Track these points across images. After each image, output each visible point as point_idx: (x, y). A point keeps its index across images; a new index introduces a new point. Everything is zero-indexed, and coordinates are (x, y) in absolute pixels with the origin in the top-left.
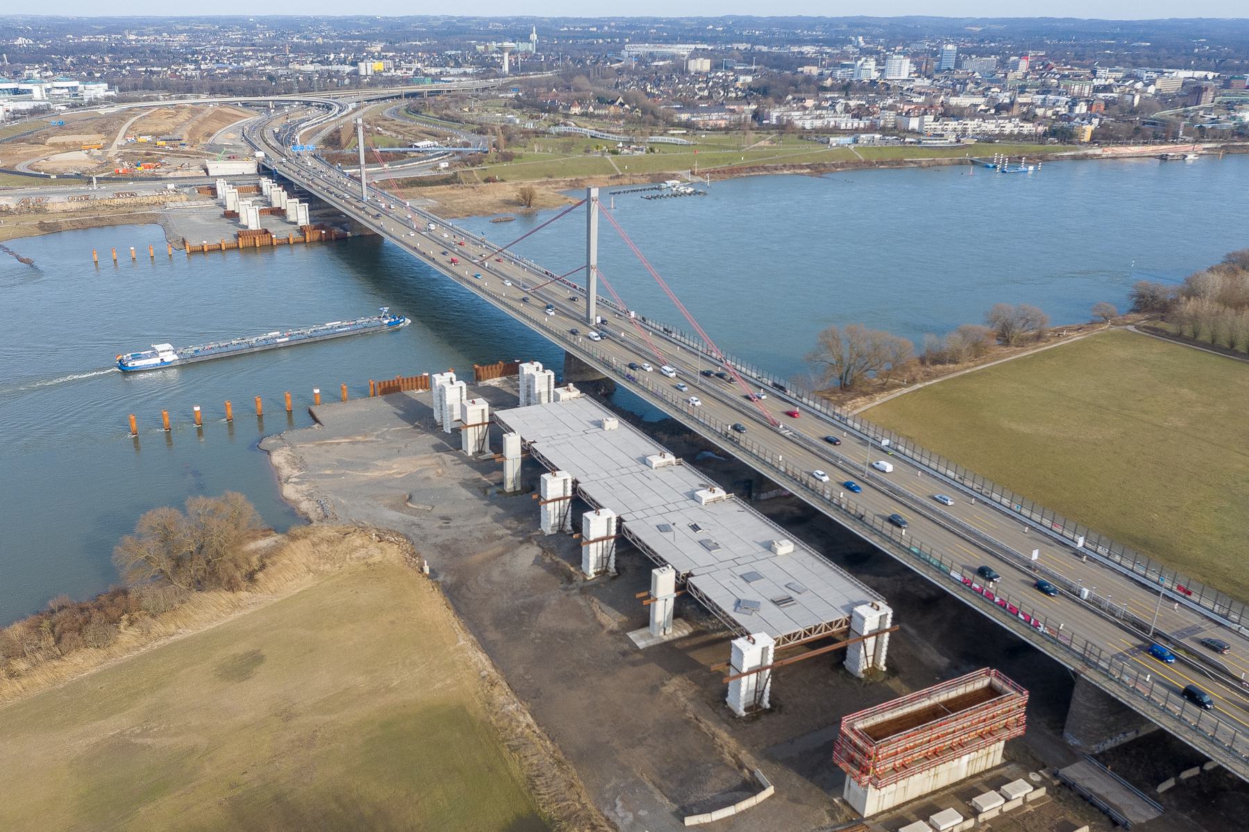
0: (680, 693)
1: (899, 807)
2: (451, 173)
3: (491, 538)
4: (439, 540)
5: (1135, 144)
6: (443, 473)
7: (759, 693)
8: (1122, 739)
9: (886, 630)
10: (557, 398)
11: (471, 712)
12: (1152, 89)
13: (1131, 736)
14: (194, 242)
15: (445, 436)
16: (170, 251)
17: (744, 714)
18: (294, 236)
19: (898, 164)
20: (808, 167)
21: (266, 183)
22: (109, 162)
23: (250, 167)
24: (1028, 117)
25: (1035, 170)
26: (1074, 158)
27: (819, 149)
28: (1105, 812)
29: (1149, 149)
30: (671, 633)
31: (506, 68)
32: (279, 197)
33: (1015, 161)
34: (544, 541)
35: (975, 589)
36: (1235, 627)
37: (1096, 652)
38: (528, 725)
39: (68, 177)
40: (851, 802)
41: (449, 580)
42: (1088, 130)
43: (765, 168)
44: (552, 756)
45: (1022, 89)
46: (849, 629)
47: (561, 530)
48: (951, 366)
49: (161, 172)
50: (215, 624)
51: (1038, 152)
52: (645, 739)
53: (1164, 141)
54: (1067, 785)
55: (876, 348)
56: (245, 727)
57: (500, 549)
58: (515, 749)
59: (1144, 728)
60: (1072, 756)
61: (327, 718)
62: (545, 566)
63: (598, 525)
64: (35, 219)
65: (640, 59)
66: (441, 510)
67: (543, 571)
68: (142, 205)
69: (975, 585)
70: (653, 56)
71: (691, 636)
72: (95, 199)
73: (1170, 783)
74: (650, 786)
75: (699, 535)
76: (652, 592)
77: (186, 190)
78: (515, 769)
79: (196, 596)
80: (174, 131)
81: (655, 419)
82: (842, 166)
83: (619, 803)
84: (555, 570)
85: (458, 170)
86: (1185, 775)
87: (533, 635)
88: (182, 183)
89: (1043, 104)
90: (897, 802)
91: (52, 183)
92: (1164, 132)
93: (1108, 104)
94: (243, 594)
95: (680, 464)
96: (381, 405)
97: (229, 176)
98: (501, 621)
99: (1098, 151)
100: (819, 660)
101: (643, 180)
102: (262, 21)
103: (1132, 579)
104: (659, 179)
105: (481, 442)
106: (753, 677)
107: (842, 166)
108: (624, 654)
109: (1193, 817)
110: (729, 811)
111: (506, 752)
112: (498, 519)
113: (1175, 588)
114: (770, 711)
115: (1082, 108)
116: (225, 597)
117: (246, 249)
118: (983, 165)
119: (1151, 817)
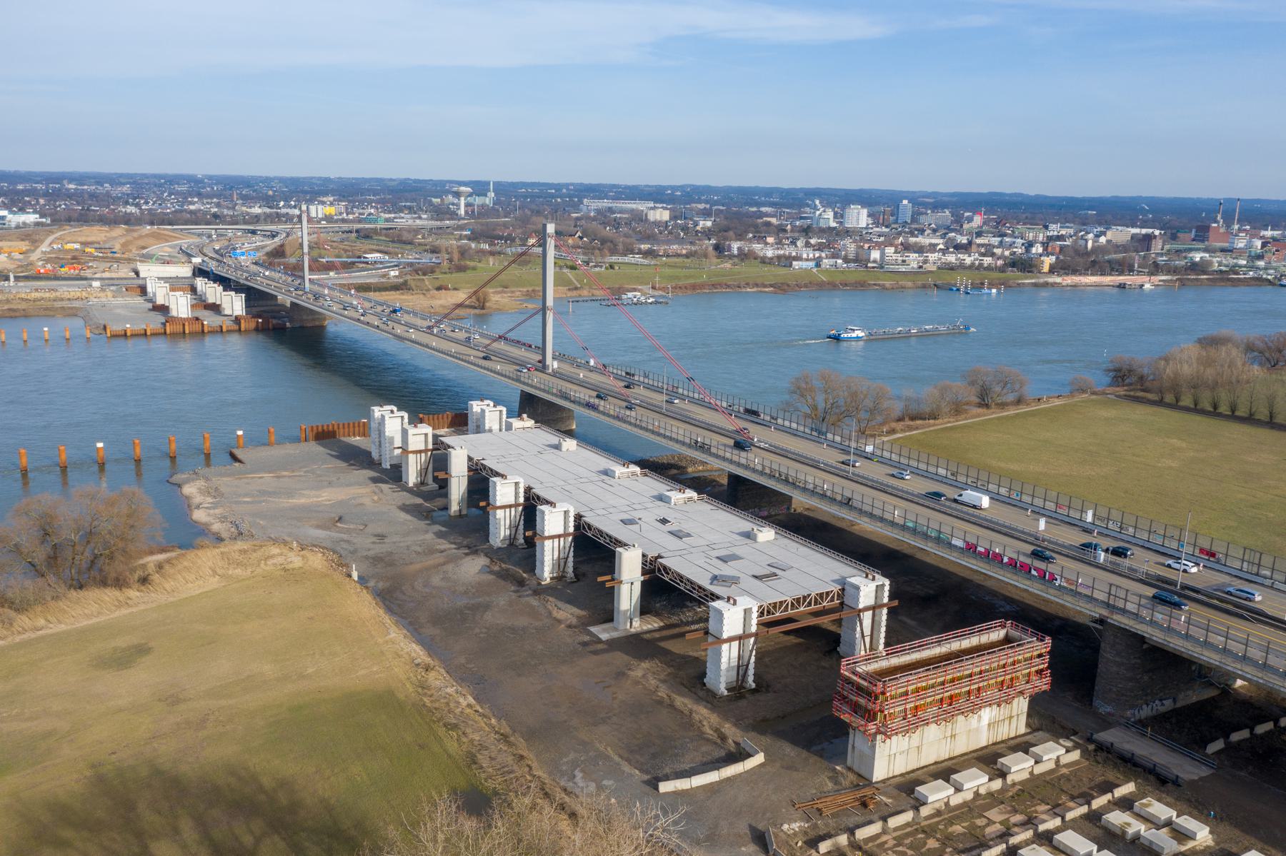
0: (650, 677)
1: (913, 771)
3: (431, 551)
4: (371, 553)
5: (1092, 275)
6: (380, 503)
7: (741, 668)
9: (884, 605)
10: (509, 427)
11: (401, 696)
12: (1103, 240)
14: (116, 327)
15: (384, 471)
16: (89, 335)
17: (726, 693)
18: (227, 324)
19: (861, 286)
20: (771, 286)
21: (200, 283)
22: (31, 264)
23: (185, 271)
24: (989, 251)
25: (999, 293)
26: (1035, 285)
27: (782, 271)
29: (1107, 279)
30: (637, 625)
31: (462, 212)
32: (213, 292)
34: (493, 554)
35: (980, 553)
36: (1268, 582)
37: (1122, 594)
38: (469, 706)
40: (855, 768)
41: (381, 585)
42: (1048, 261)
43: (728, 286)
44: (497, 733)
45: (979, 234)
46: (842, 604)
47: (512, 540)
48: (932, 421)
49: (88, 273)
50: (95, 620)
52: (609, 718)
53: (1121, 273)
55: (854, 395)
56: (120, 710)
57: (442, 560)
58: (454, 727)
60: (1106, 723)
61: (223, 702)
62: (492, 572)
63: (554, 522)
65: (598, 211)
66: (373, 528)
67: (492, 577)
68: (62, 300)
69: (979, 549)
70: (610, 210)
71: (661, 629)
72: (10, 292)
74: (616, 758)
75: (668, 527)
76: (616, 576)
78: (452, 746)
79: (74, 594)
80: (105, 242)
82: (806, 286)
83: (579, 775)
84: (504, 576)
85: (409, 277)
86: (1236, 737)
87: (477, 630)
88: (107, 283)
89: (1001, 245)
90: (910, 768)
92: (1123, 267)
93: (1062, 248)
94: (133, 593)
96: (314, 448)
98: (437, 620)
99: (1058, 280)
100: (808, 640)
104: (618, 292)
105: (423, 472)
106: (735, 644)
107: (806, 286)
108: (585, 644)
109: (1250, 774)
111: (441, 731)
112: (440, 535)
114: (753, 691)
115: (1038, 249)
116: (109, 595)
117: (173, 335)
118: (949, 288)
119: (1204, 774)
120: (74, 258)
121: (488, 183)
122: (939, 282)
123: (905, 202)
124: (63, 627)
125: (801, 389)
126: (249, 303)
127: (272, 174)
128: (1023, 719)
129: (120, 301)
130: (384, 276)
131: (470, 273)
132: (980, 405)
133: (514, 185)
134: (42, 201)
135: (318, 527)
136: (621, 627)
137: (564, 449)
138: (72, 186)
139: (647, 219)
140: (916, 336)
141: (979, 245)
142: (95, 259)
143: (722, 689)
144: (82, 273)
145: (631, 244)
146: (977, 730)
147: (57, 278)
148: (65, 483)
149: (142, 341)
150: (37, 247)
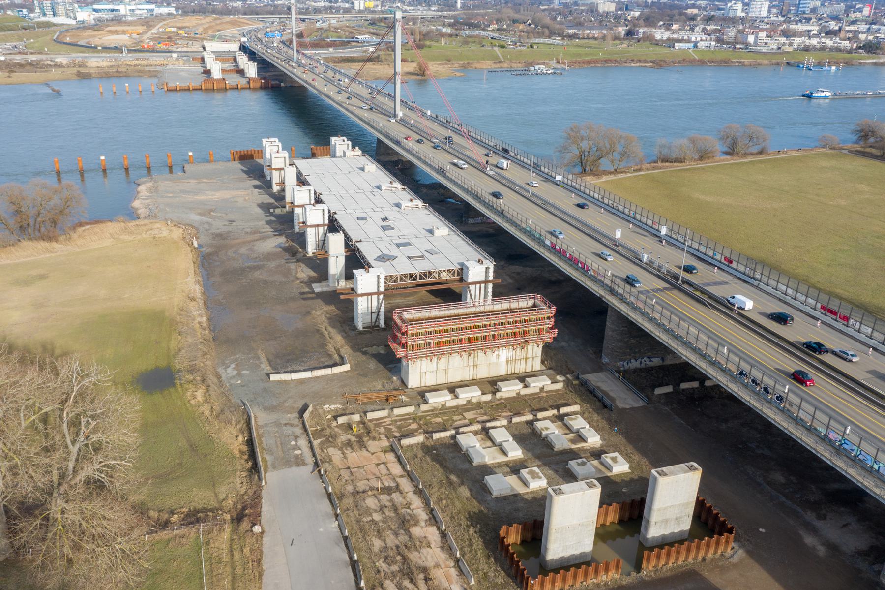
2: (375, 55)
8: (646, 362)
9: (490, 282)
13: (656, 362)
14: (172, 85)
19: (725, 63)
20: (651, 62)
25: (838, 69)
26: (875, 64)
28: (600, 400)
30: (490, 305)
31: (459, 5)
32: (243, 60)
33: (820, 64)
36: (756, 283)
39: (109, 48)
43: (617, 62)
51: (844, 59)
54: (584, 384)
59: (669, 357)
60: (599, 368)
64: (75, 70)
73: (669, 389)
77: (185, 58)
80: (194, 27)
81: (428, 182)
82: (679, 62)
86: (684, 386)
91: (99, 52)
95: (404, 189)
96: (237, 165)
101: (519, 65)
107: (679, 62)
110: (307, 375)
112: (269, 223)
113: (723, 260)
114: (384, 329)
117: (207, 90)
119: (636, 406)
120: (169, 38)
124: (9, 262)
126: (260, 70)
129: (187, 67)
130: (365, 51)
135: (200, 214)
136: (331, 285)
137: (366, 170)
139: (597, 10)
141: (848, 31)
142: (182, 38)
143: (360, 327)
145: (563, 30)
146: (497, 364)
147: (153, 51)
148: (83, 180)
150: (149, 30)
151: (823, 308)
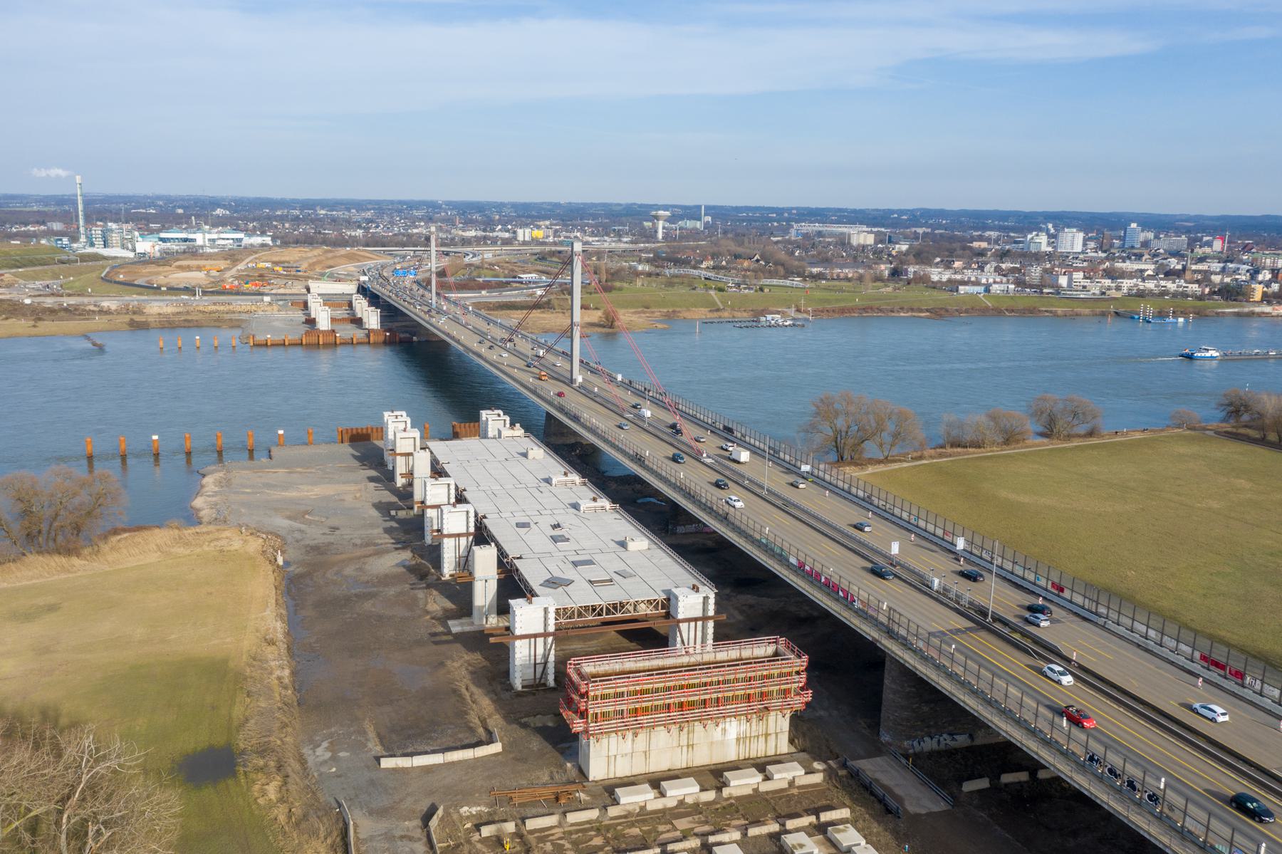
2: (545, 299)
9: (710, 618)
14: (260, 338)
20: (927, 310)
25: (1187, 321)
26: (1238, 314)
27: (944, 296)
31: (660, 235)
42: (1258, 290)
43: (880, 310)
54: (855, 775)
60: (877, 750)
70: (820, 234)
73: (983, 784)
81: (617, 473)
82: (967, 311)
85: (552, 297)
86: (1007, 778)
89: (1223, 270)
95: (584, 484)
96: (346, 449)
97: (328, 292)
99: (1268, 309)
102: (449, 203)
103: (1009, 581)
107: (967, 311)
110: (437, 759)
113: (1049, 587)
114: (553, 689)
117: (309, 346)
118: (1131, 317)
119: (936, 809)
121: (699, 207)
122: (1121, 310)
123: (1134, 225)
125: (825, 409)
126: (384, 319)
127: (506, 200)
128: (785, 738)
129: (283, 314)
130: (531, 295)
131: (614, 294)
132: (1043, 435)
133: (738, 209)
134: (287, 225)
135: (289, 518)
137: (530, 457)
138: (323, 212)
140: (1274, 358)
142: (279, 276)
144: (262, 290)
146: (722, 743)
149: (349, 348)
151: (1204, 658)
